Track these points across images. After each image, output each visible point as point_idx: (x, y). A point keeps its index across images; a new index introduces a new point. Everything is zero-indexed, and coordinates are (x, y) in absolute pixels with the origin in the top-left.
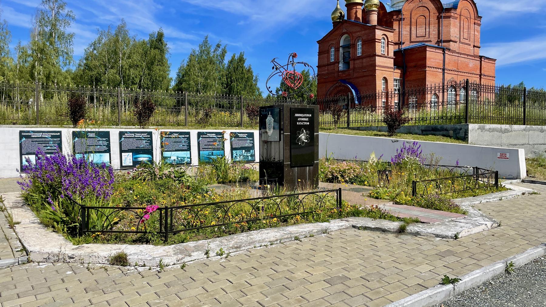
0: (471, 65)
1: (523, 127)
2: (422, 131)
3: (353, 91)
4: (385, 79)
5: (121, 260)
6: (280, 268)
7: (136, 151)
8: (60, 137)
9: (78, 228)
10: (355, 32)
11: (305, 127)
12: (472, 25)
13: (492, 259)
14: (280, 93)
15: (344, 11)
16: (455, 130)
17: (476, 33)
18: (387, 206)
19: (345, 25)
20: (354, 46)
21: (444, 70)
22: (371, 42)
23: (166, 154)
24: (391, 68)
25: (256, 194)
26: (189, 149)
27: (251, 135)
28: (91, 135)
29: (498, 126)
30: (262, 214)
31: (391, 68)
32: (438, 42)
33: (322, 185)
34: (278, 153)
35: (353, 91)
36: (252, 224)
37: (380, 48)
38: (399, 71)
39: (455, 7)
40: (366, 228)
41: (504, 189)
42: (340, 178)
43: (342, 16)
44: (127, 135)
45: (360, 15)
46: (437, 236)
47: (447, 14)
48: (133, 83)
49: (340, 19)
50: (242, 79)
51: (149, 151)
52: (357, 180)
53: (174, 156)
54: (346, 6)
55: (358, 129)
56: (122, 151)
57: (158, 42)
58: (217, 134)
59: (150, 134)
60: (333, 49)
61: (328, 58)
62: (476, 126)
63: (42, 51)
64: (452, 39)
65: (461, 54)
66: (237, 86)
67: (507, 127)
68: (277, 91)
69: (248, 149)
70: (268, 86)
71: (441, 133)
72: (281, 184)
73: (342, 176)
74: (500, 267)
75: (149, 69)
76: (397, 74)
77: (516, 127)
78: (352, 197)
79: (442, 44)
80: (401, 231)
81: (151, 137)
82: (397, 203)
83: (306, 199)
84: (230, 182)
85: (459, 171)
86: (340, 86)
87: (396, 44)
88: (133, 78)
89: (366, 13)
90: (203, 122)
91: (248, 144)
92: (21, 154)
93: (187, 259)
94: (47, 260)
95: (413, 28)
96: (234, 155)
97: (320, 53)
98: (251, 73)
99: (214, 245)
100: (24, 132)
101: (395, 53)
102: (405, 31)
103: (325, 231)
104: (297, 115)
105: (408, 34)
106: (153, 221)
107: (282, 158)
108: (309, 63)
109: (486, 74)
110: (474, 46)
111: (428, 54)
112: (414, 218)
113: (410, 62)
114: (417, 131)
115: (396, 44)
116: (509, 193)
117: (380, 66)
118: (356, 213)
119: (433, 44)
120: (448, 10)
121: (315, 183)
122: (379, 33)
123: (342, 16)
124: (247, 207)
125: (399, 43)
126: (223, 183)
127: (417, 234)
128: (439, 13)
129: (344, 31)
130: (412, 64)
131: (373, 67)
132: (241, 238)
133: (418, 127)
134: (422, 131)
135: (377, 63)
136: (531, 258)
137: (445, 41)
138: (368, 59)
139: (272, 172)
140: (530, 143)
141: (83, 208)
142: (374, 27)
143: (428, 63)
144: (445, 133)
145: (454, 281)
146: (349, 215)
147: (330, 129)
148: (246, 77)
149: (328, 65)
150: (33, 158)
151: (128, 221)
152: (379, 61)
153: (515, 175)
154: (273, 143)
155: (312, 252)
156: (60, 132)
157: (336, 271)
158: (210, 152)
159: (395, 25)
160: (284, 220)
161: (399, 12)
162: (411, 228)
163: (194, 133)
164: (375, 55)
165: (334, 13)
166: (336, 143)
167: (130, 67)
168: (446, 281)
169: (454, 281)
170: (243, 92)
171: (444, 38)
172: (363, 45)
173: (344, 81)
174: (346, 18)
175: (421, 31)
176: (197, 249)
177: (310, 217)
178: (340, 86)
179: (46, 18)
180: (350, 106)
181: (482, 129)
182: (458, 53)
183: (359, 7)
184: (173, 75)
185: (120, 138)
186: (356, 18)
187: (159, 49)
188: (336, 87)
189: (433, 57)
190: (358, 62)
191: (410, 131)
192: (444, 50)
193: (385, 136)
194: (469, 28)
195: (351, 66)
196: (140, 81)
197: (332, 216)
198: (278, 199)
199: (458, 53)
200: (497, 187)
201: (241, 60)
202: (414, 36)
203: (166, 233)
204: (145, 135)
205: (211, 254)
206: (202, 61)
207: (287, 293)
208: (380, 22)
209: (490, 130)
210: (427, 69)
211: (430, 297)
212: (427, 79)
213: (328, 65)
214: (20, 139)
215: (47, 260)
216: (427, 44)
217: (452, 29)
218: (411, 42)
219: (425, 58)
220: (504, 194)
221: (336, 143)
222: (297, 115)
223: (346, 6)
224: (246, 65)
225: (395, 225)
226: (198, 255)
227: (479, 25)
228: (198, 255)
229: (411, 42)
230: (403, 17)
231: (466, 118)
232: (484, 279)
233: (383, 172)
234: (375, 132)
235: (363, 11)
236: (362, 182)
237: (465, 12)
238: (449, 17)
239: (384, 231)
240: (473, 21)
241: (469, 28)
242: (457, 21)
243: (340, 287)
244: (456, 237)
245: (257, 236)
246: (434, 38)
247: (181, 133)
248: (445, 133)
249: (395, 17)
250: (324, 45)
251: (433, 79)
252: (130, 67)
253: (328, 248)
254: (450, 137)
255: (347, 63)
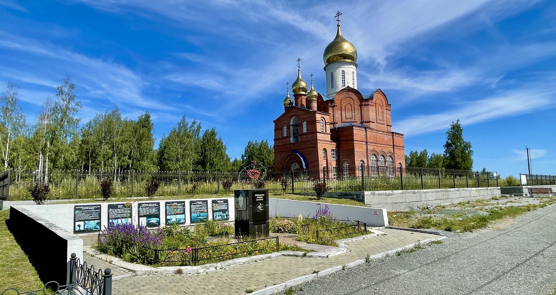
0: (386, 139)
1: (401, 191)
2: (339, 196)
3: (301, 158)
4: (325, 150)
5: (179, 272)
6: (248, 272)
7: (149, 216)
8: (100, 208)
9: (154, 261)
10: (301, 115)
11: (260, 201)
12: (385, 111)
13: (338, 264)
14: (245, 158)
15: (293, 100)
16: (357, 195)
17: (388, 115)
18: (299, 244)
19: (293, 110)
20: (301, 125)
21: (367, 142)
22: (313, 123)
23: (168, 217)
24: (329, 141)
25: (234, 241)
26: (184, 213)
27: (226, 201)
28: (119, 206)
29: (384, 192)
30: (239, 251)
31: (329, 141)
32: (361, 123)
33: (271, 234)
34: (245, 216)
35: (301, 158)
36: (234, 256)
37: (319, 127)
38: (335, 144)
39: (371, 98)
40: (288, 255)
41: (371, 233)
42: (283, 230)
43: (291, 103)
44: (143, 205)
45: (304, 102)
46: (320, 257)
47: (366, 103)
48: (125, 155)
49: (290, 105)
50: (214, 149)
51: (158, 216)
52: (293, 231)
53: (173, 218)
54: (294, 96)
55: (299, 194)
56: (139, 216)
57: (145, 123)
58: (203, 201)
59: (158, 204)
60: (285, 127)
61: (282, 133)
62: (369, 192)
63: (54, 133)
64: (371, 120)
65: (378, 131)
66: (211, 155)
67: (390, 192)
68: (242, 157)
69: (224, 211)
70: (235, 153)
71: (350, 197)
72: (248, 235)
73: (284, 229)
74: (340, 267)
75: (138, 144)
76: (333, 146)
77: (396, 192)
78: (285, 239)
79: (364, 124)
80: (304, 255)
81: (159, 206)
82: (309, 243)
83: (261, 242)
84: (216, 235)
85: (350, 223)
86: (291, 155)
87: (331, 124)
88: (125, 151)
89: (309, 102)
90: (192, 192)
91: (224, 207)
92: (75, 221)
93: (208, 270)
94: (144, 274)
95: (343, 113)
96: (215, 216)
97: (276, 130)
98: (222, 144)
99: (219, 265)
100: (77, 206)
101: (331, 130)
102: (338, 115)
103: (269, 258)
104: (256, 195)
105: (341, 116)
106: (189, 255)
107: (248, 218)
108: (266, 136)
109: (397, 145)
110: (387, 125)
111: (355, 132)
112: (312, 249)
113: (342, 137)
114: (335, 196)
115: (331, 124)
116: (372, 235)
117: (320, 140)
118: (286, 249)
119: (358, 124)
120: (367, 100)
121: (267, 234)
122: (318, 116)
123: (291, 103)
124: (230, 248)
125: (333, 123)
126: (212, 236)
127: (311, 256)
128: (361, 102)
129: (293, 114)
130: (345, 139)
131: (315, 140)
132: (230, 262)
133: (336, 193)
134: (339, 196)
135: (318, 138)
136: (357, 264)
137: (366, 122)
138: (312, 135)
139: (242, 227)
140: (407, 201)
141: (156, 250)
142: (315, 112)
143: (355, 138)
144: (351, 197)
145: (317, 272)
146: (282, 250)
147: (280, 195)
148: (217, 147)
149: (282, 139)
150: (82, 223)
151: (176, 256)
152: (319, 136)
153: (382, 224)
154: (243, 212)
155: (251, 276)
156: (100, 205)
157: (272, 271)
158: (198, 213)
159: (330, 111)
160: (250, 254)
161: (332, 101)
162: (308, 254)
163: (187, 202)
164: (316, 132)
165: (285, 101)
166: (283, 206)
167: (122, 142)
168: (315, 272)
169: (317, 272)
170: (215, 159)
171: (365, 120)
172: (307, 124)
173: (295, 151)
174: (294, 105)
175: (349, 115)
176: (211, 266)
177: (263, 252)
178: (291, 155)
179: (59, 107)
180: (295, 175)
181: (374, 194)
182: (376, 130)
183: (303, 97)
184: (156, 147)
185: (139, 208)
186: (302, 104)
187: (146, 127)
188: (289, 155)
189: (358, 133)
190: (304, 137)
191: (331, 196)
192: (366, 128)
193: (315, 199)
194: (383, 113)
195: (299, 140)
196: (130, 153)
197: (273, 251)
198: (246, 243)
199: (376, 130)
200: (366, 232)
201: (213, 134)
202: (344, 118)
203: (195, 261)
204: (155, 205)
205: (218, 268)
206: (181, 135)
207: (251, 279)
208: (319, 109)
209: (379, 195)
210: (355, 142)
211: (306, 278)
212: (355, 149)
213: (282, 139)
214: (75, 211)
215: (144, 274)
216: (353, 124)
217: (371, 113)
218: (342, 122)
219: (352, 135)
220: (369, 236)
221: (283, 206)
222: (256, 195)
223: (294, 96)
224: (217, 137)
225: (301, 253)
226: (212, 269)
227: (390, 110)
228: (212, 269)
229: (342, 122)
230: (335, 104)
231: (362, 188)
232: (332, 272)
233: (306, 224)
234: (310, 197)
235: (306, 99)
236: (295, 232)
237: (378, 101)
238: (368, 105)
239: (297, 256)
240: (385, 107)
241: (383, 113)
242: (374, 107)
243: (272, 276)
244: (327, 257)
245: (237, 260)
246: (358, 120)
247: (178, 202)
248: (351, 197)
249: (330, 104)
250: (279, 124)
251: (359, 150)
252: (122, 142)
253: (270, 264)
254: (355, 200)
255: (296, 137)
